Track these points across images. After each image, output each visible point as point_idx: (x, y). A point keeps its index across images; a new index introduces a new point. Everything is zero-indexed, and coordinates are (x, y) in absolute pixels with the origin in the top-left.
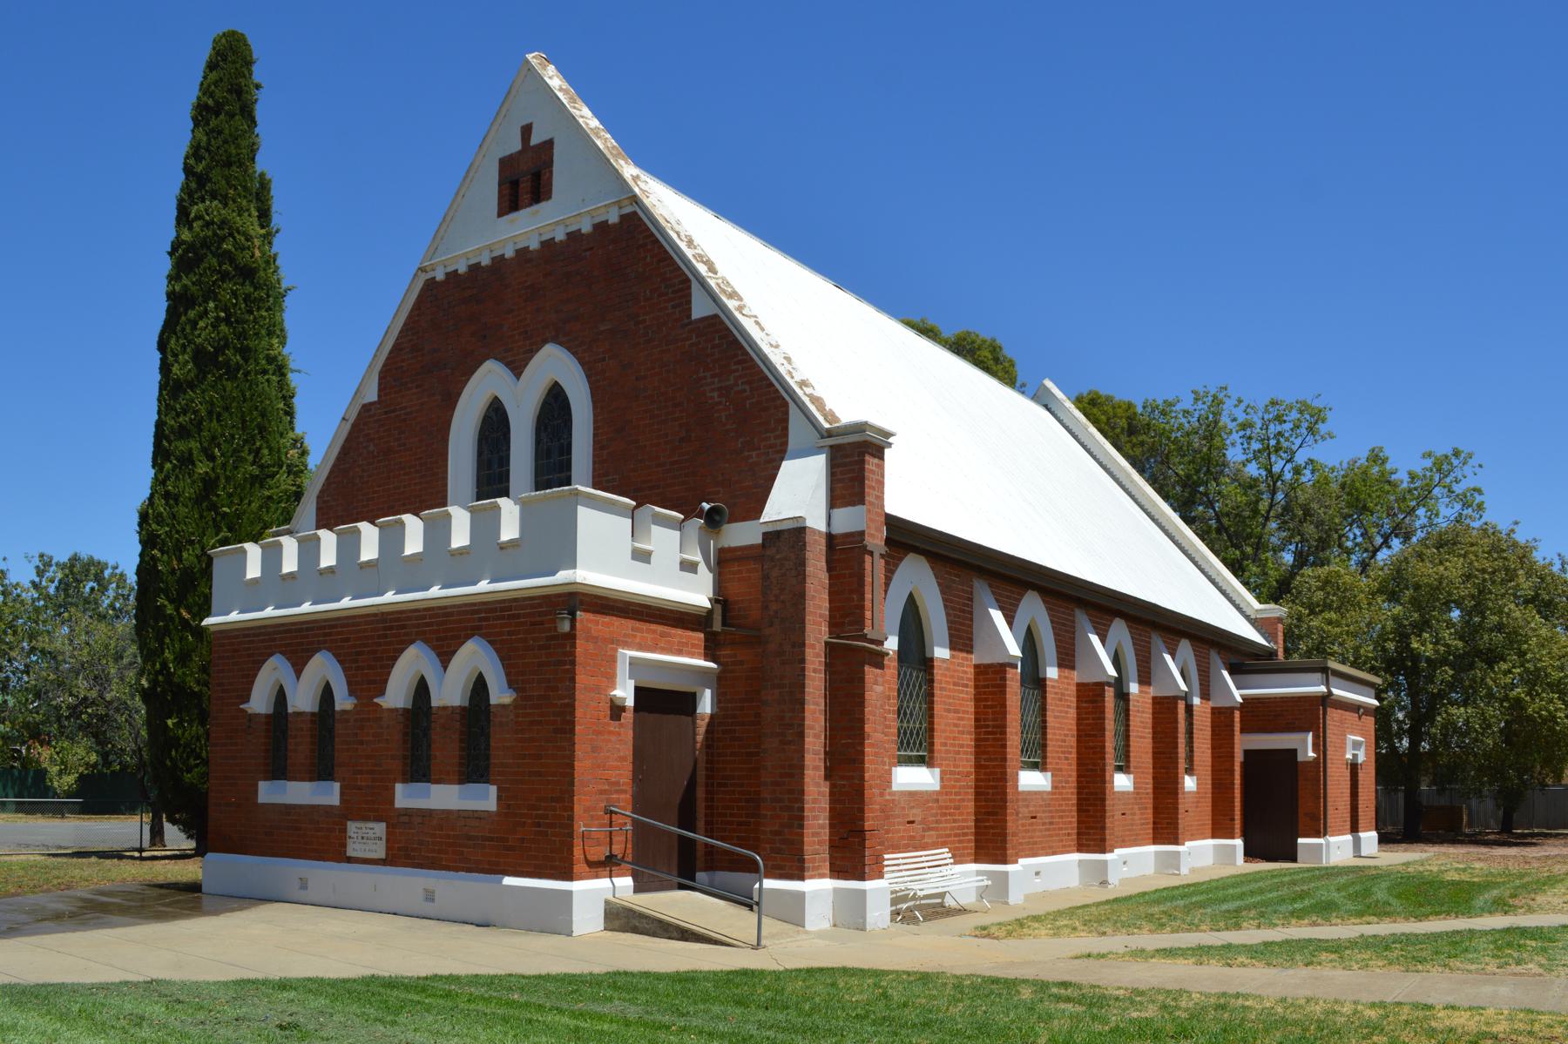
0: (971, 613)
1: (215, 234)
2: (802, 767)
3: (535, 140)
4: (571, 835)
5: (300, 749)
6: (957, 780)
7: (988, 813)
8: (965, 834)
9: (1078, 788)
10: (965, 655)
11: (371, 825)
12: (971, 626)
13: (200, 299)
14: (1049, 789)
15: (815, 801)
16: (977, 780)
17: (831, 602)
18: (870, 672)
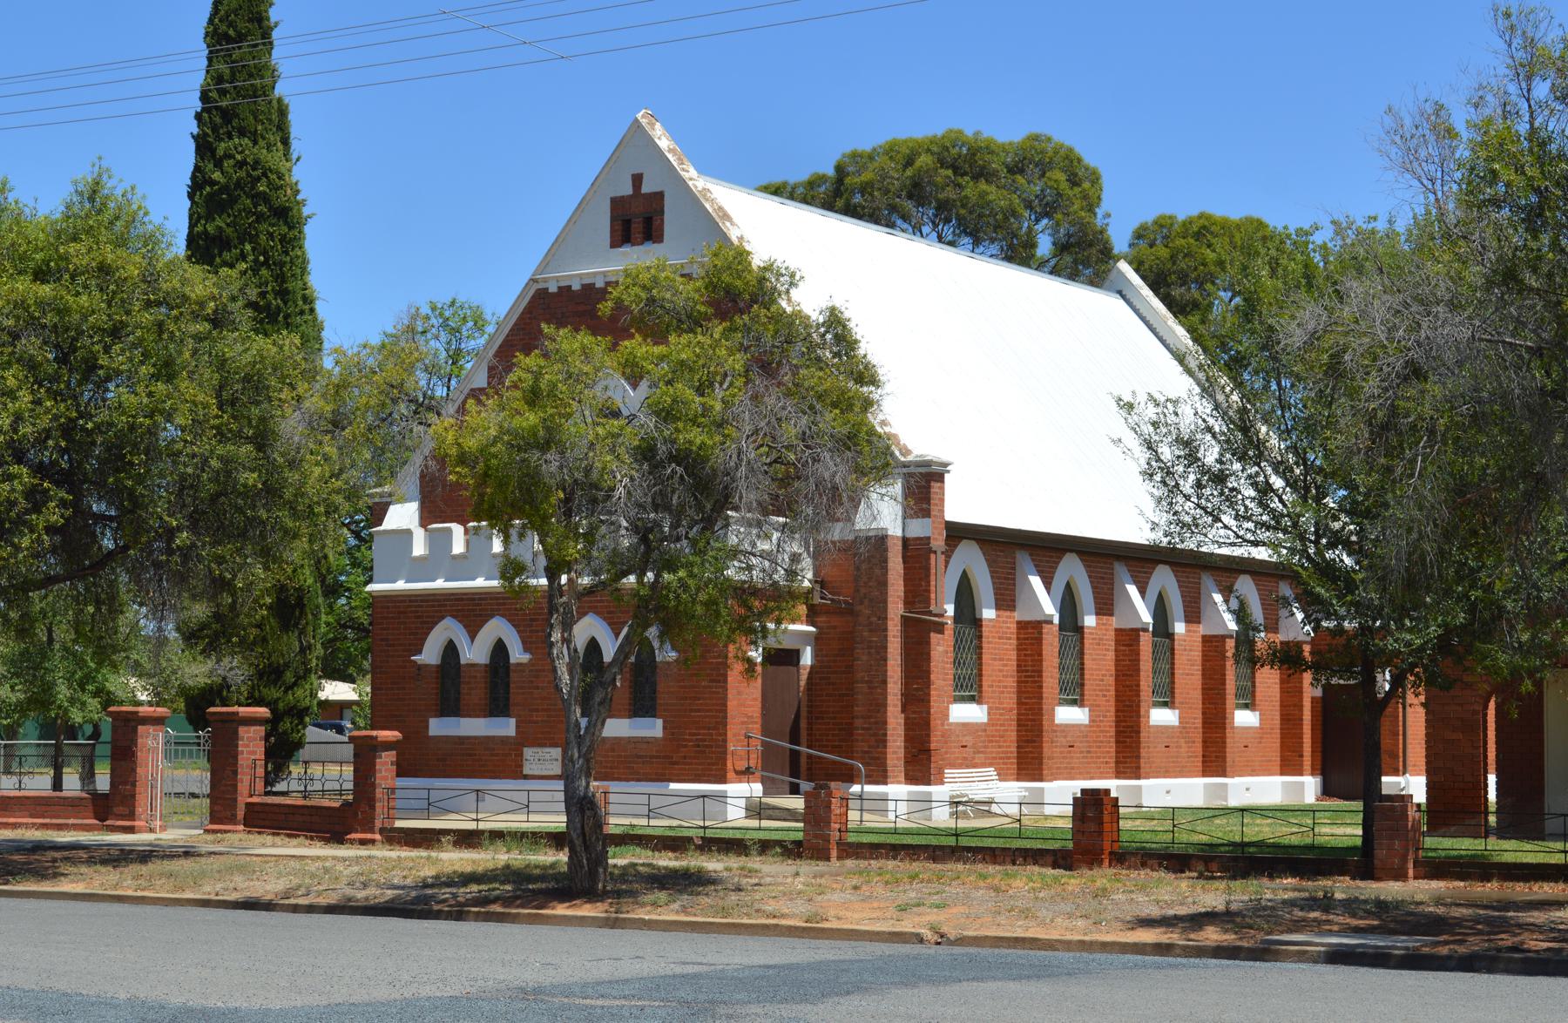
0: (1014, 579)
1: (249, 175)
2: (885, 705)
3: (645, 189)
4: (725, 753)
5: (475, 692)
6: (1001, 714)
7: (1028, 741)
8: (1009, 758)
9: (1117, 722)
10: (1008, 613)
11: (547, 750)
12: (1014, 590)
13: (236, 241)
14: (1087, 722)
15: (894, 729)
16: (1018, 714)
17: (905, 586)
18: (934, 637)
